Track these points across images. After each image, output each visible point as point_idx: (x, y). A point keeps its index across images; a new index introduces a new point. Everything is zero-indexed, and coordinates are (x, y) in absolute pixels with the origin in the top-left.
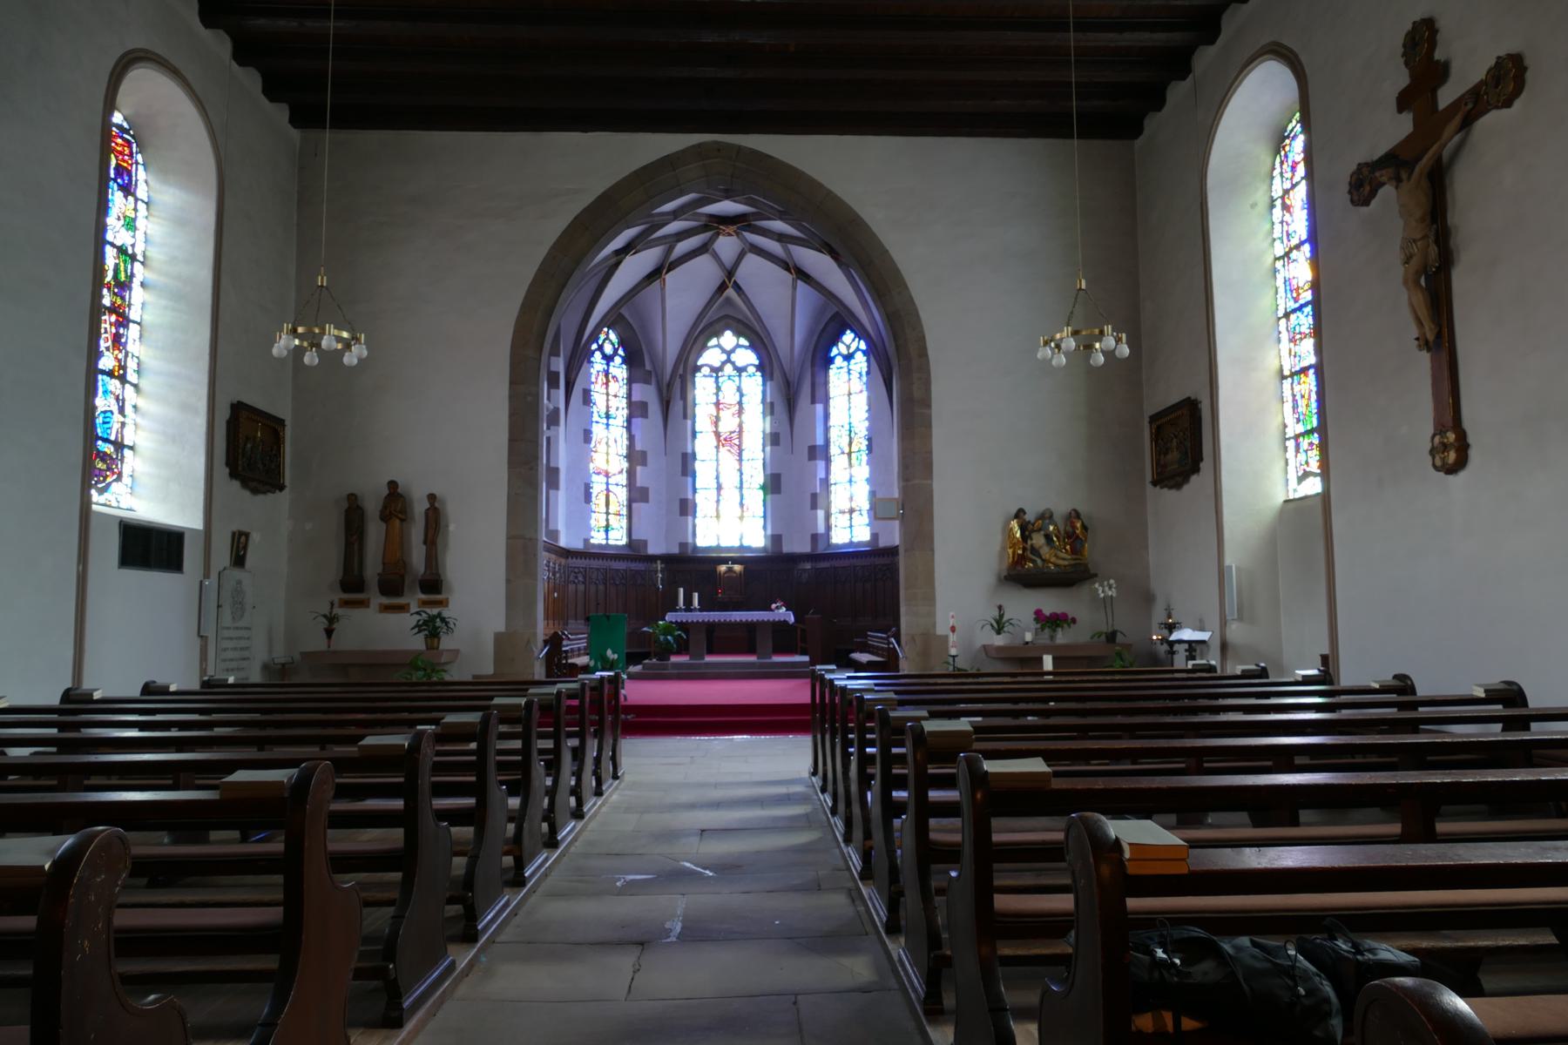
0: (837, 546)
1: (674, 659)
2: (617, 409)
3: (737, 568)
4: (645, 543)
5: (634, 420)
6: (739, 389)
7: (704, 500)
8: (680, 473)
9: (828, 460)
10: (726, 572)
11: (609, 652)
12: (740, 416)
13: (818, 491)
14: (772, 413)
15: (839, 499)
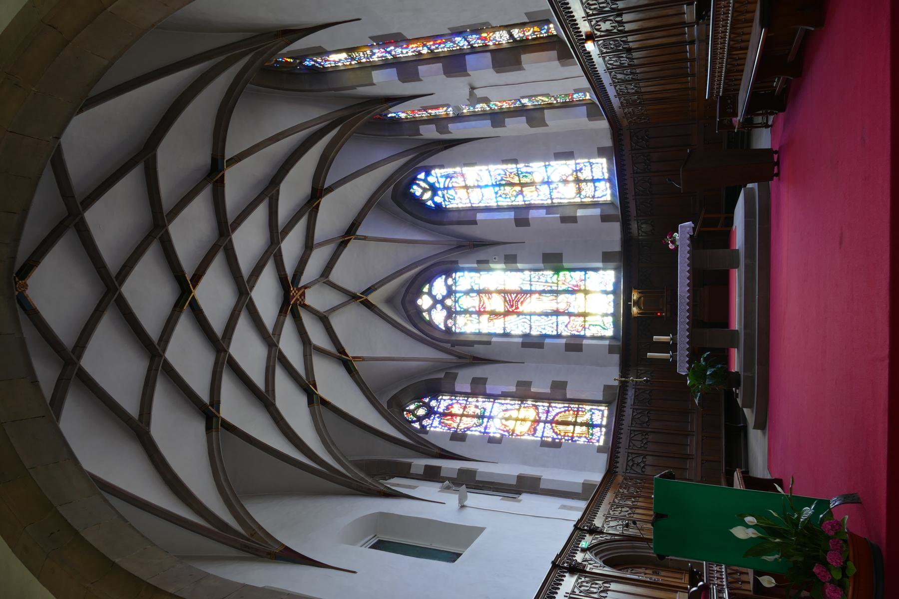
0: (613, 195)
1: (736, 365)
2: (477, 407)
3: (635, 296)
4: (607, 388)
5: (488, 392)
6: (467, 293)
7: (568, 327)
9: (529, 207)
10: (639, 308)
11: (740, 532)
13: (559, 215)
14: (487, 262)
15: (567, 194)
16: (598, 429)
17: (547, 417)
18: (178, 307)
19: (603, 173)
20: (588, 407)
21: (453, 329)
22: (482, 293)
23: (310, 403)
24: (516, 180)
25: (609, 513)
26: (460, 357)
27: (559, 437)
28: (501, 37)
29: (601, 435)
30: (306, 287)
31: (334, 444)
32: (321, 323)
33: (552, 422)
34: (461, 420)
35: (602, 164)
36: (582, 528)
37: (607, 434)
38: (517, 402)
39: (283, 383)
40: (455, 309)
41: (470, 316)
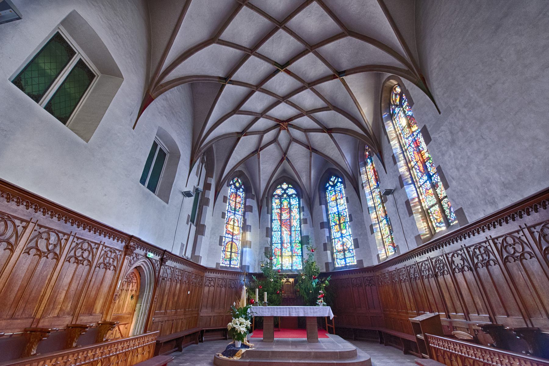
0: (339, 268)
3: (291, 280)
6: (289, 203)
9: (330, 228)
12: (290, 213)
16: (229, 263)
17: (234, 239)
19: (349, 263)
20: (239, 258)
21: (274, 198)
22: (290, 210)
24: (342, 221)
26: (261, 201)
27: (225, 245)
28: (430, 201)
29: (226, 265)
30: (288, 130)
32: (273, 139)
33: (232, 241)
34: (234, 201)
35: (354, 262)
36: (165, 255)
37: (226, 267)
38: (242, 226)
40: (283, 199)
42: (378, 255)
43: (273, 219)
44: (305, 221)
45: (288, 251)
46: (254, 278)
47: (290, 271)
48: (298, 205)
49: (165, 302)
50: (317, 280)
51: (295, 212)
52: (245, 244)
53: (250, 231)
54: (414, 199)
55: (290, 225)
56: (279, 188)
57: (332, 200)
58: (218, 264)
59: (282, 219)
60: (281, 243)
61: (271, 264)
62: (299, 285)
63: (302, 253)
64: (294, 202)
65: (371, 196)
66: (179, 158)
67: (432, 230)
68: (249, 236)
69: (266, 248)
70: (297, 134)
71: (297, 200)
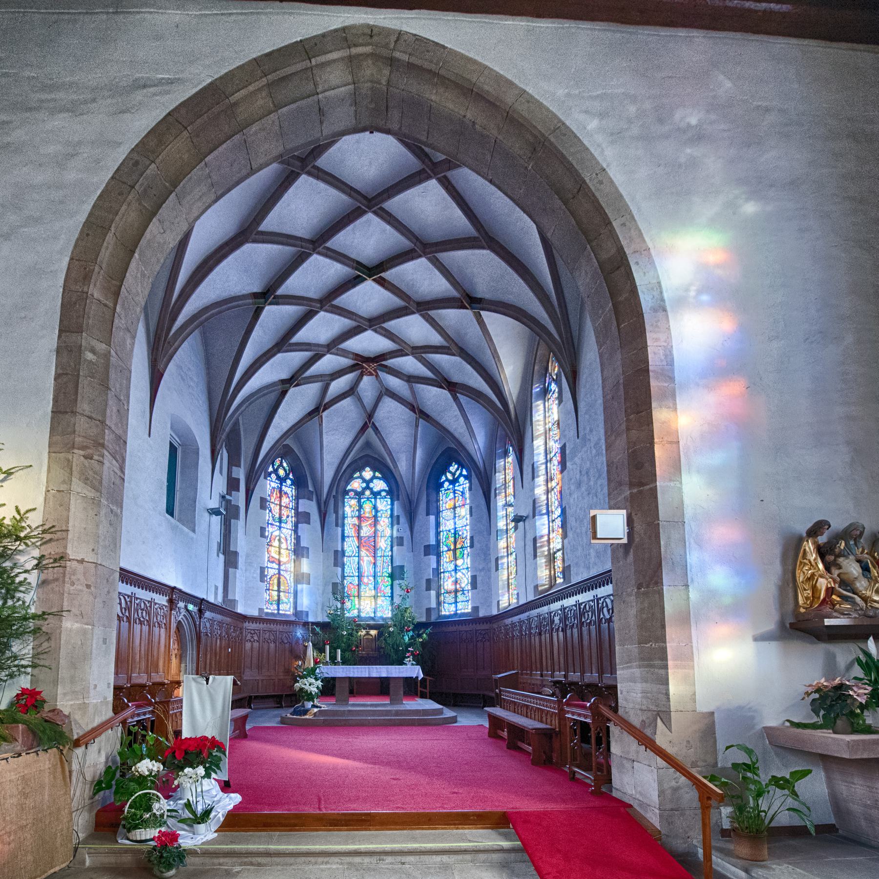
2: (288, 517)
3: (373, 632)
8: (333, 565)
9: (439, 555)
12: (375, 526)
18: (358, 265)
20: (292, 600)
21: (347, 497)
23: (283, 381)
24: (458, 546)
25: (215, 621)
26: (325, 503)
30: (377, 376)
31: (250, 404)
33: (279, 573)
36: (202, 604)
37: (272, 614)
39: (297, 358)
41: (357, 510)
42: (498, 602)
43: (346, 535)
44: (400, 541)
45: (370, 589)
46: (318, 629)
47: (373, 619)
48: (389, 512)
49: (208, 661)
50: (411, 633)
51: (384, 522)
52: (299, 578)
53: (308, 557)
54: (542, 537)
55: (374, 546)
56: (357, 478)
57: (447, 507)
58: (261, 610)
59: (362, 535)
60: (358, 576)
61: (342, 609)
62: (385, 640)
63: (392, 593)
64: (384, 505)
65: (505, 512)
66: (198, 453)
67: (552, 579)
68: (305, 566)
69: (335, 585)
70: (393, 382)
71: (389, 503)
